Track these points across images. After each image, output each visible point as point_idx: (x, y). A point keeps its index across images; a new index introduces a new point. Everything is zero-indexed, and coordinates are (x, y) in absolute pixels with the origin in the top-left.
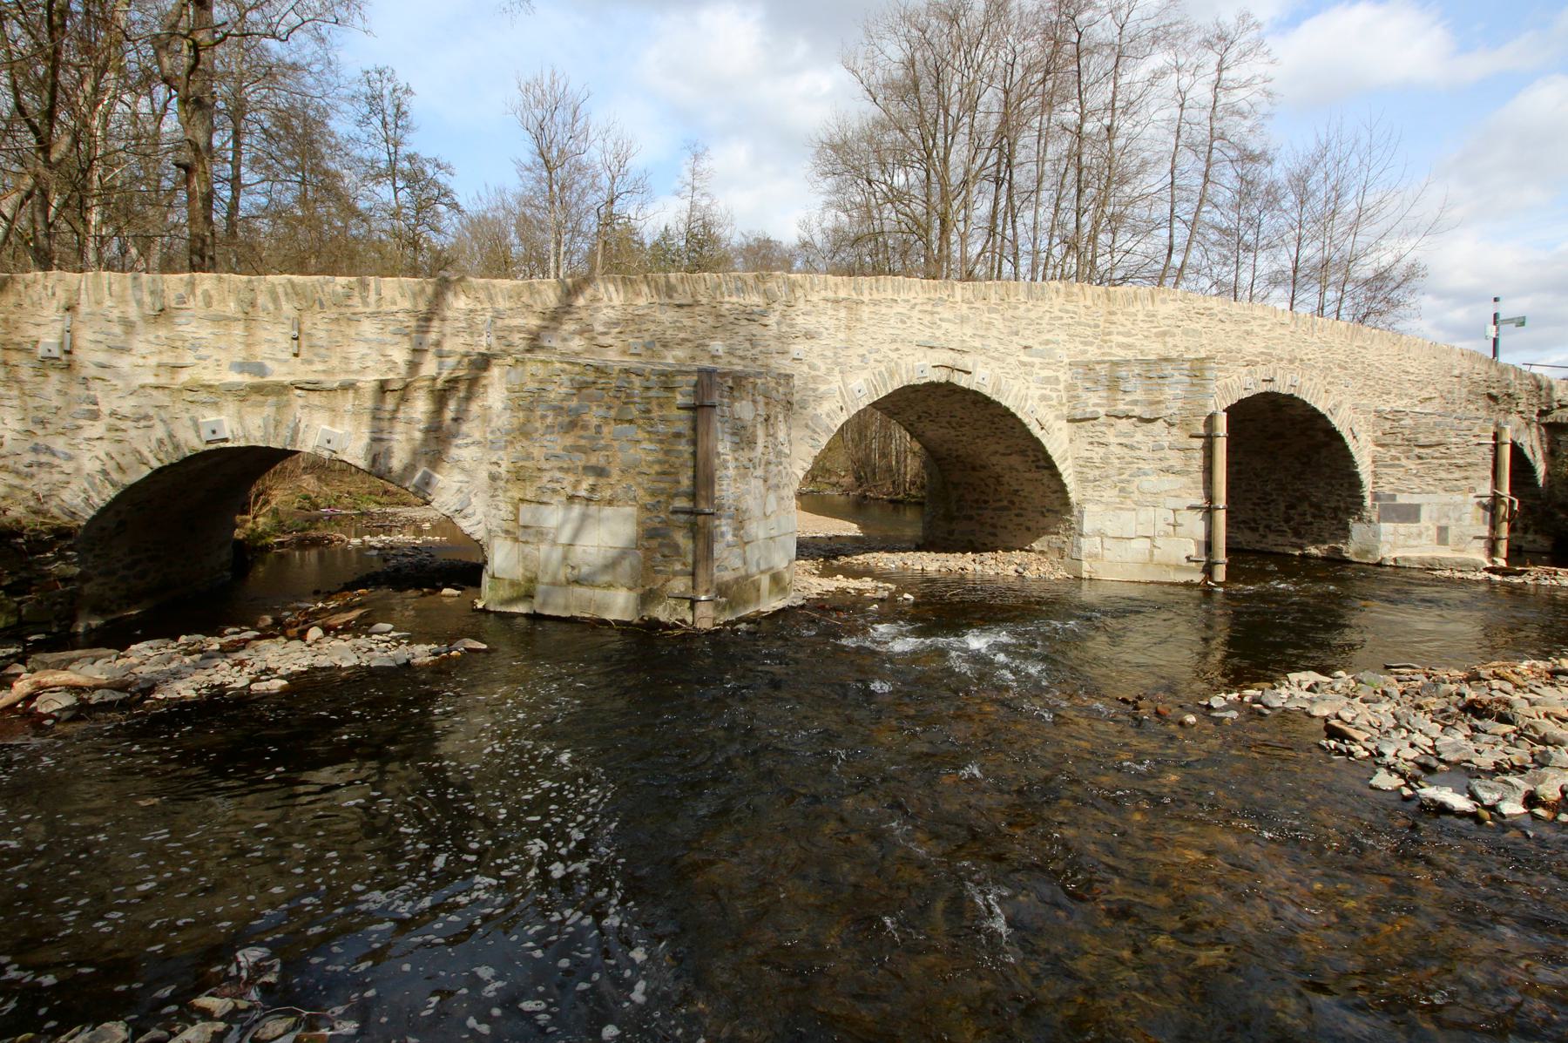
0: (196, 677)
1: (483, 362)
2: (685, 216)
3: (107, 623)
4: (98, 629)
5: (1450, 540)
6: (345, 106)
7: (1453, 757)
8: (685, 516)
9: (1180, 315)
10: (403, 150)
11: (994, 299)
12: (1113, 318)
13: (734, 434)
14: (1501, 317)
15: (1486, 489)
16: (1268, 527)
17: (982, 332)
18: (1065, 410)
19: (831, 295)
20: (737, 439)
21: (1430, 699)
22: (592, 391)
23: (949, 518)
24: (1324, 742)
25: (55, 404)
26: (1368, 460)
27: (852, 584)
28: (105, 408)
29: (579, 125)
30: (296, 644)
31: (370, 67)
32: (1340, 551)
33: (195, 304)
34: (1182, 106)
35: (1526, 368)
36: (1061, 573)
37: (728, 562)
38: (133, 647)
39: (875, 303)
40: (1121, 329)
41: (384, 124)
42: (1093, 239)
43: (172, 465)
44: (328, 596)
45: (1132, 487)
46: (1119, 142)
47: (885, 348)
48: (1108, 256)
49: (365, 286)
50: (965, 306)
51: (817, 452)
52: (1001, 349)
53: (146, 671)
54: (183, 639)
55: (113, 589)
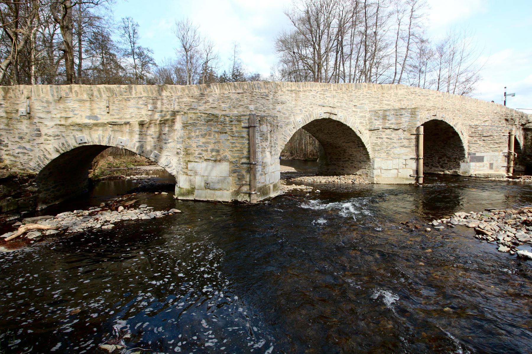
0: (82, 225)
1: (174, 114)
2: (232, 67)
3: (48, 207)
4: (45, 209)
5: (494, 168)
6: (116, 31)
7: (524, 240)
8: (249, 165)
9: (405, 94)
10: (136, 46)
11: (344, 89)
12: (384, 95)
13: (261, 137)
14: (507, 94)
15: (506, 150)
16: (432, 165)
17: (340, 101)
18: (368, 127)
19: (290, 89)
20: (262, 138)
21: (510, 220)
22: (212, 123)
23: (327, 165)
24: (477, 236)
25: (25, 132)
26: (466, 142)
27: (298, 187)
28: (43, 133)
29: (196, 37)
30: (115, 212)
31: (124, 17)
32: (456, 172)
33: (73, 96)
34: (399, 24)
35: (517, 110)
36: (367, 182)
37: (261, 180)
38: (58, 215)
39: (305, 91)
40: (386, 99)
41: (130, 36)
42: (370, 70)
43: (67, 152)
44: (122, 196)
45: (391, 152)
46: (378, 37)
47: (308, 107)
48: (375, 76)
49: (131, 88)
50: (334, 92)
51: (286, 143)
52: (347, 106)
53: (64, 223)
54: (75, 211)
55: (49, 195)
